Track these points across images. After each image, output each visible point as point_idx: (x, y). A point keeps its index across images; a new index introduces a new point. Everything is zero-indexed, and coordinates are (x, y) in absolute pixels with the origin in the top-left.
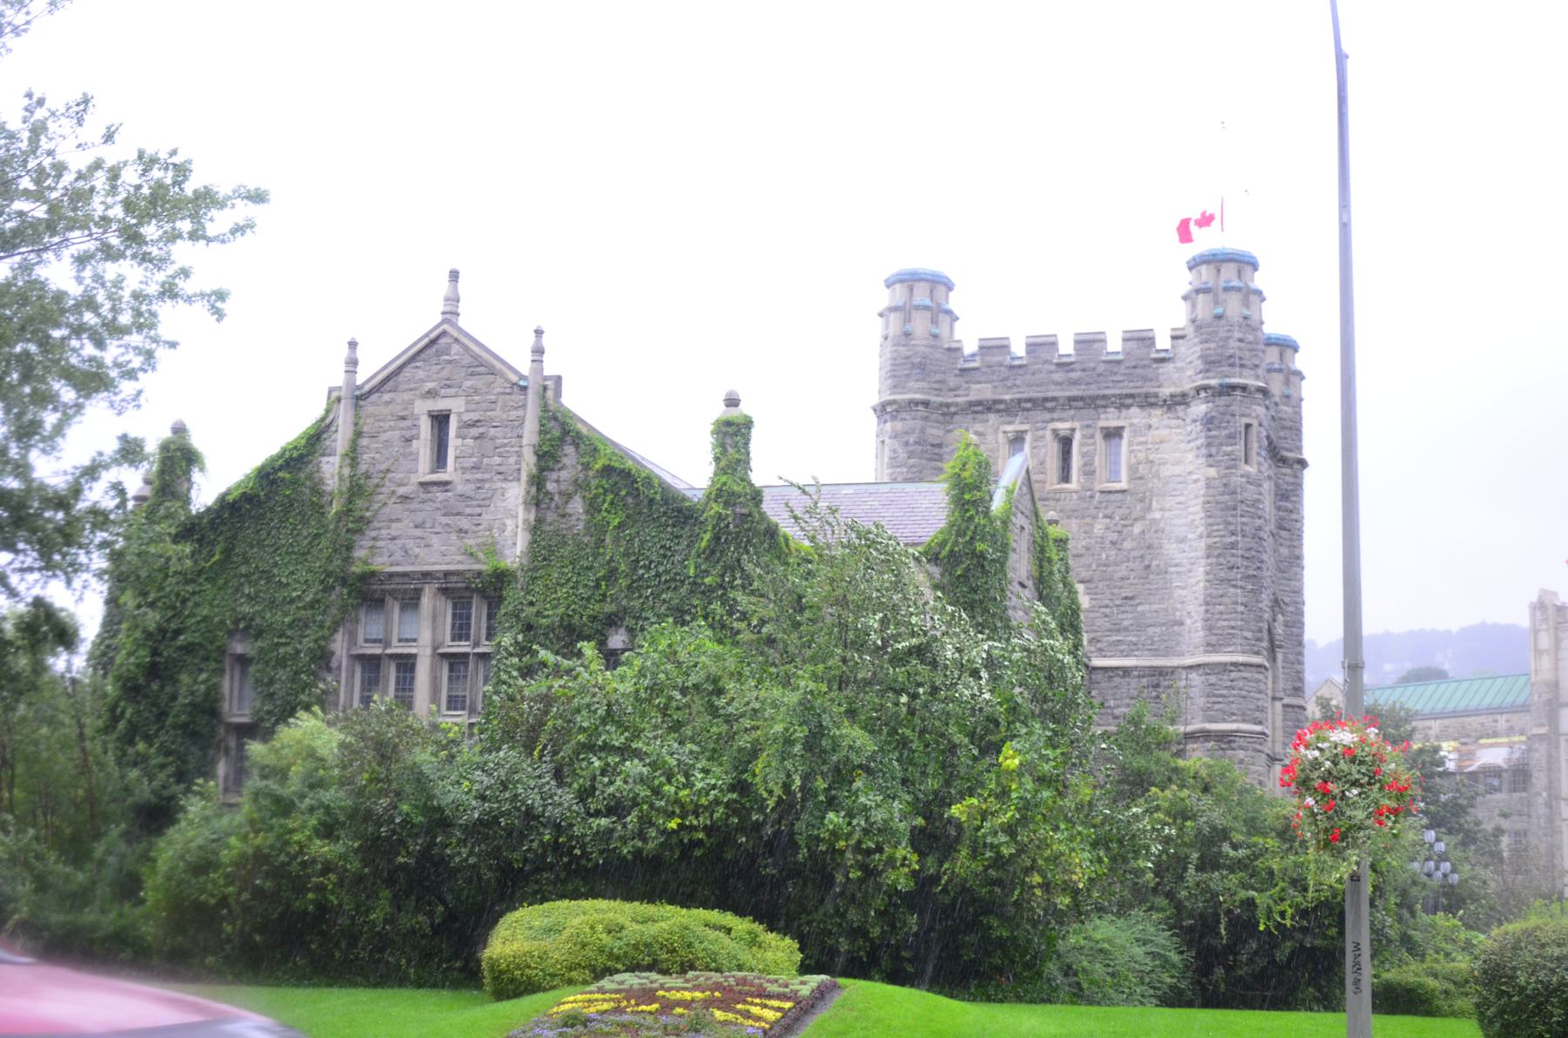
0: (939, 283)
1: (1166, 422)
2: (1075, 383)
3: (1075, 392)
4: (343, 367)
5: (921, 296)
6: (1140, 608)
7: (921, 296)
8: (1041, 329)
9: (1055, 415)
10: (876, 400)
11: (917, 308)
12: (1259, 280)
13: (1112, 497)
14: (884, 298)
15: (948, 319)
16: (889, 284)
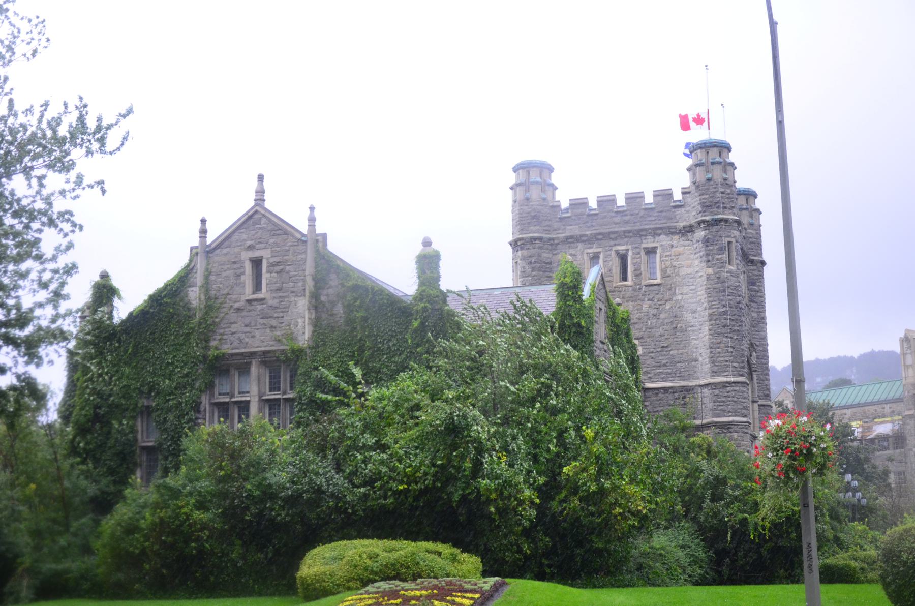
0: (545, 169)
1: (682, 242)
2: (627, 222)
3: (628, 228)
4: (198, 235)
5: (533, 177)
6: (672, 352)
7: (533, 177)
8: (606, 192)
9: (617, 242)
10: (511, 238)
11: (533, 183)
12: (732, 157)
13: (651, 288)
14: (512, 179)
15: (551, 189)
16: (516, 170)
